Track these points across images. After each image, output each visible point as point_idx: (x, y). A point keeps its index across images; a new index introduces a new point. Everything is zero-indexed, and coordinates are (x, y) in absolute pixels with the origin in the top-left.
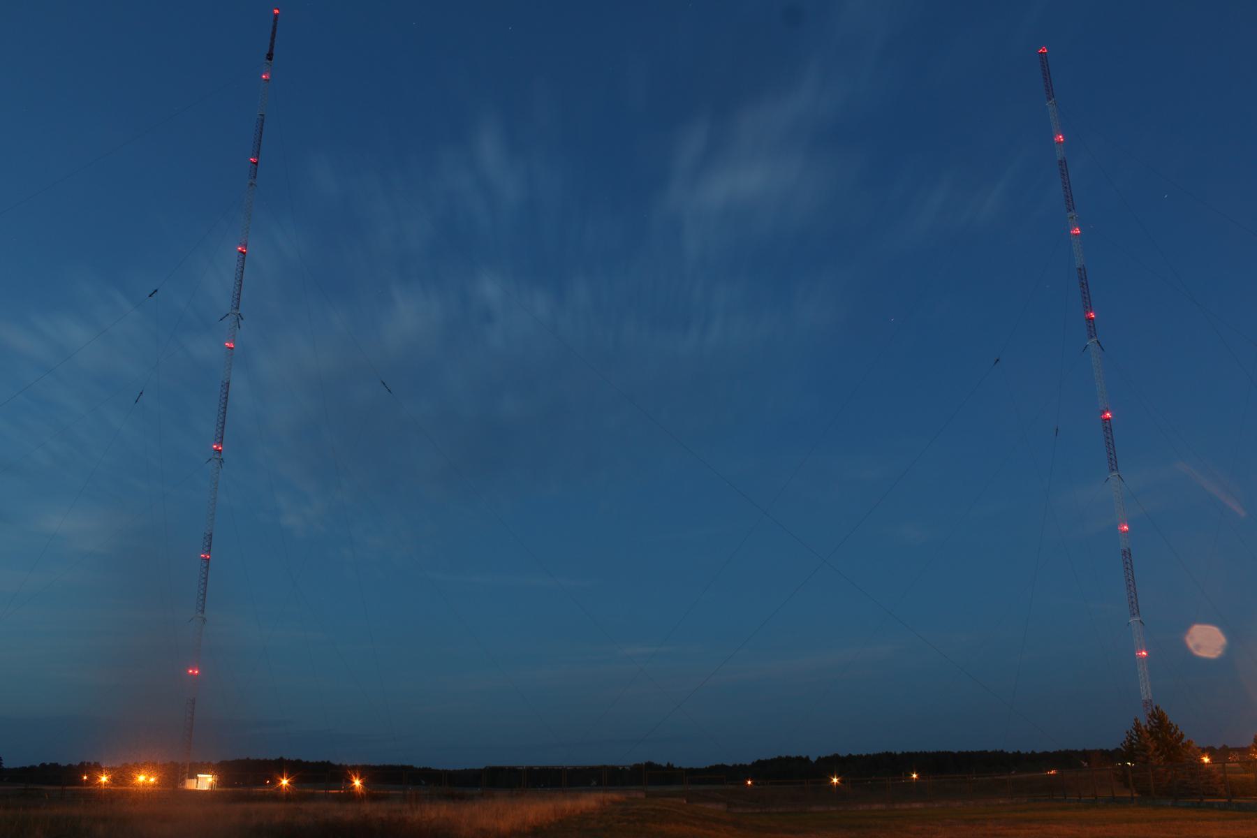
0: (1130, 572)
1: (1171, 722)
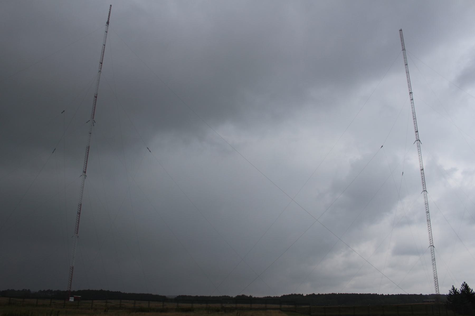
0: (430, 227)
1: (470, 288)
